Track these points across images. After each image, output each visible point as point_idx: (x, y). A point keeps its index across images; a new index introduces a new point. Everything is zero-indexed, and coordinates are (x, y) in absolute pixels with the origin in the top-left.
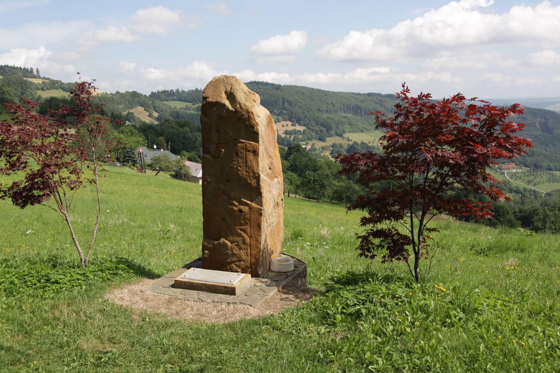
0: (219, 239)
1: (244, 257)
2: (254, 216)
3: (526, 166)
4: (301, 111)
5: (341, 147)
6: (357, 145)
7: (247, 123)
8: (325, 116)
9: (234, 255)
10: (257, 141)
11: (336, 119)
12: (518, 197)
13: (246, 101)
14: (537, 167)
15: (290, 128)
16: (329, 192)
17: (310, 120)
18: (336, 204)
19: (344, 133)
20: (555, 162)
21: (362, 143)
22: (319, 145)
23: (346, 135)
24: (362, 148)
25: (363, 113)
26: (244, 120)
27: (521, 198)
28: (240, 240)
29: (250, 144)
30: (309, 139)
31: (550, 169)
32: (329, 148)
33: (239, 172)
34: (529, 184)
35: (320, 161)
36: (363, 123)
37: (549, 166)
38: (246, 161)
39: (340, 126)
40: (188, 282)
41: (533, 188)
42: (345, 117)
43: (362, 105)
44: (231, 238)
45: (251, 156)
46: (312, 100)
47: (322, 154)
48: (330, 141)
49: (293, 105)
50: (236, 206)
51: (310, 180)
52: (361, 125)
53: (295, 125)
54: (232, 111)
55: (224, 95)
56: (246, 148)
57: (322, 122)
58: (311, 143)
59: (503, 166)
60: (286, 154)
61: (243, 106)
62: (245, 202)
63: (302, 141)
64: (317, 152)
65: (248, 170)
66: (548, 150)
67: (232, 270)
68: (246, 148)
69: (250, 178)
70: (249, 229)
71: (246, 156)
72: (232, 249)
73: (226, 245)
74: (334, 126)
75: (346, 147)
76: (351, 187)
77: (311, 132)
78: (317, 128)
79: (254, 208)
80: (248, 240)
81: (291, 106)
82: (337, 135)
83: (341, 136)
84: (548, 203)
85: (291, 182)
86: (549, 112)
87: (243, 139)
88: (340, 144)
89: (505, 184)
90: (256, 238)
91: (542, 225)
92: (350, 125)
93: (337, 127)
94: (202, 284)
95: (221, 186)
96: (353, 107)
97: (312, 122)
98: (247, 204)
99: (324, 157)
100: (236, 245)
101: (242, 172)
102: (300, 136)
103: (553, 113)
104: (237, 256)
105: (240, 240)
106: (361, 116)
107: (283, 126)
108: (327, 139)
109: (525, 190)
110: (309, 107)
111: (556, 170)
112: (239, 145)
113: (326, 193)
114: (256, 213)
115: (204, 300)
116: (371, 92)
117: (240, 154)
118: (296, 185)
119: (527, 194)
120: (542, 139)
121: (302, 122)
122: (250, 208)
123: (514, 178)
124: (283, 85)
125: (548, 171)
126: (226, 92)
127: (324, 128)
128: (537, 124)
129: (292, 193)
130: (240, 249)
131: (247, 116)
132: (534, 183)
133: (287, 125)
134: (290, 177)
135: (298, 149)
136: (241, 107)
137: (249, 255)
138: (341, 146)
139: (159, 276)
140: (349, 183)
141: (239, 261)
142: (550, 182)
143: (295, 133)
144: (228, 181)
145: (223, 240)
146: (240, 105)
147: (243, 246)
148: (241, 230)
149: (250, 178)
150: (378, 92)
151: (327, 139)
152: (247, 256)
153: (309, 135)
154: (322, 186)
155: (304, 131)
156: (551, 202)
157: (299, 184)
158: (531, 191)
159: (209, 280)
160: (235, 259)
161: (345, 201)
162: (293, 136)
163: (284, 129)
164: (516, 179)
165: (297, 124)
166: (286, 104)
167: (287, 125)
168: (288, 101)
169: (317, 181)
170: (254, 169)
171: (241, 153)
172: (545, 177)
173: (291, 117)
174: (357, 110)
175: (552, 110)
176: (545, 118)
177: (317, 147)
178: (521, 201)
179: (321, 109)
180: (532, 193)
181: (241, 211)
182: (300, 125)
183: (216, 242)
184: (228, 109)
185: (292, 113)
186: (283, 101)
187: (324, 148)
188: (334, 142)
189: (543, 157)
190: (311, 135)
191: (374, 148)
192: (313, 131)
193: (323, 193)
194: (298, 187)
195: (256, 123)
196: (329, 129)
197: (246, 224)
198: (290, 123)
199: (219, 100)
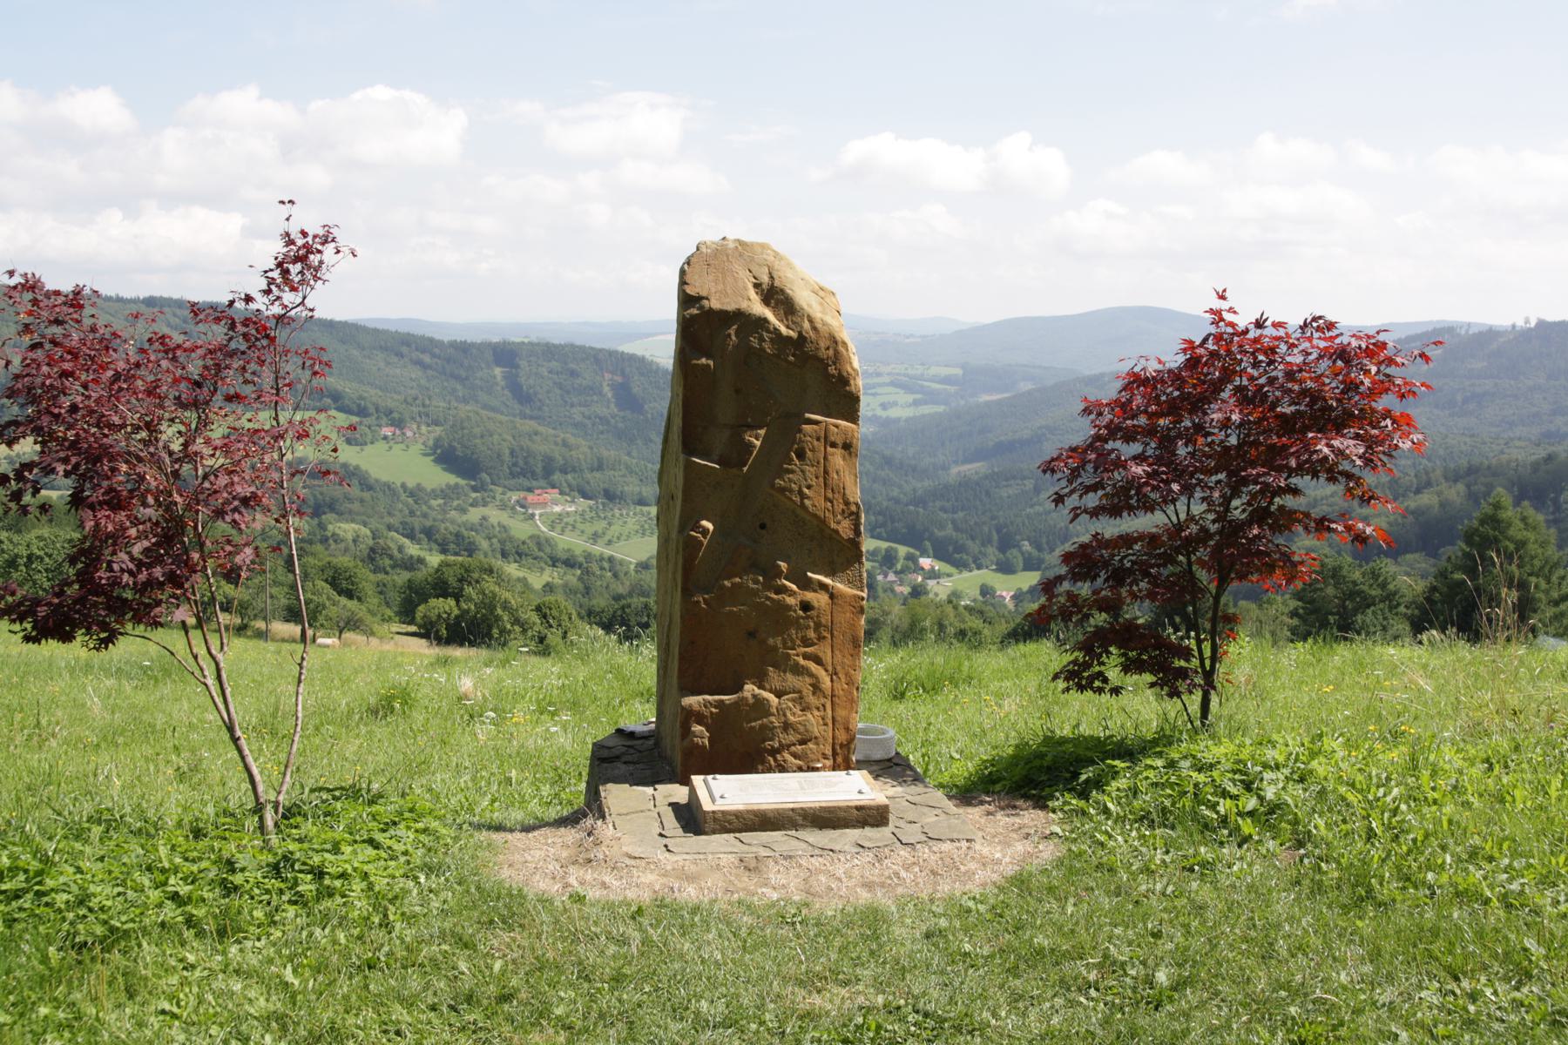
0: (741, 688)
1: (816, 730)
3: (585, 496)
7: (832, 370)
9: (787, 726)
10: (852, 416)
12: (573, 577)
13: (824, 312)
14: (611, 496)
26: (822, 364)
27: (580, 579)
28: (803, 683)
38: (826, 472)
41: (608, 552)
45: (837, 458)
50: (792, 594)
51: (17, 556)
54: (789, 338)
55: (752, 293)
59: (531, 497)
61: (819, 326)
65: (830, 495)
66: (634, 453)
67: (782, 769)
71: (825, 458)
72: (781, 712)
73: (760, 703)
79: (842, 595)
86: (632, 358)
89: (539, 545)
98: (824, 587)
100: (793, 700)
101: (816, 501)
103: (642, 360)
109: (588, 556)
112: (807, 427)
114: (848, 608)
116: (157, 294)
117: (809, 454)
119: (595, 567)
120: (621, 425)
122: (832, 596)
123: (558, 528)
126: (756, 286)
132: (607, 538)
136: (815, 329)
139: (918, 779)
141: (803, 742)
144: (763, 526)
146: (811, 321)
147: (812, 700)
148: (806, 656)
158: (602, 559)
164: (563, 532)
175: (639, 353)
176: (623, 373)
178: (581, 586)
180: (606, 565)
181: (806, 606)
197: (821, 638)
199: (744, 305)
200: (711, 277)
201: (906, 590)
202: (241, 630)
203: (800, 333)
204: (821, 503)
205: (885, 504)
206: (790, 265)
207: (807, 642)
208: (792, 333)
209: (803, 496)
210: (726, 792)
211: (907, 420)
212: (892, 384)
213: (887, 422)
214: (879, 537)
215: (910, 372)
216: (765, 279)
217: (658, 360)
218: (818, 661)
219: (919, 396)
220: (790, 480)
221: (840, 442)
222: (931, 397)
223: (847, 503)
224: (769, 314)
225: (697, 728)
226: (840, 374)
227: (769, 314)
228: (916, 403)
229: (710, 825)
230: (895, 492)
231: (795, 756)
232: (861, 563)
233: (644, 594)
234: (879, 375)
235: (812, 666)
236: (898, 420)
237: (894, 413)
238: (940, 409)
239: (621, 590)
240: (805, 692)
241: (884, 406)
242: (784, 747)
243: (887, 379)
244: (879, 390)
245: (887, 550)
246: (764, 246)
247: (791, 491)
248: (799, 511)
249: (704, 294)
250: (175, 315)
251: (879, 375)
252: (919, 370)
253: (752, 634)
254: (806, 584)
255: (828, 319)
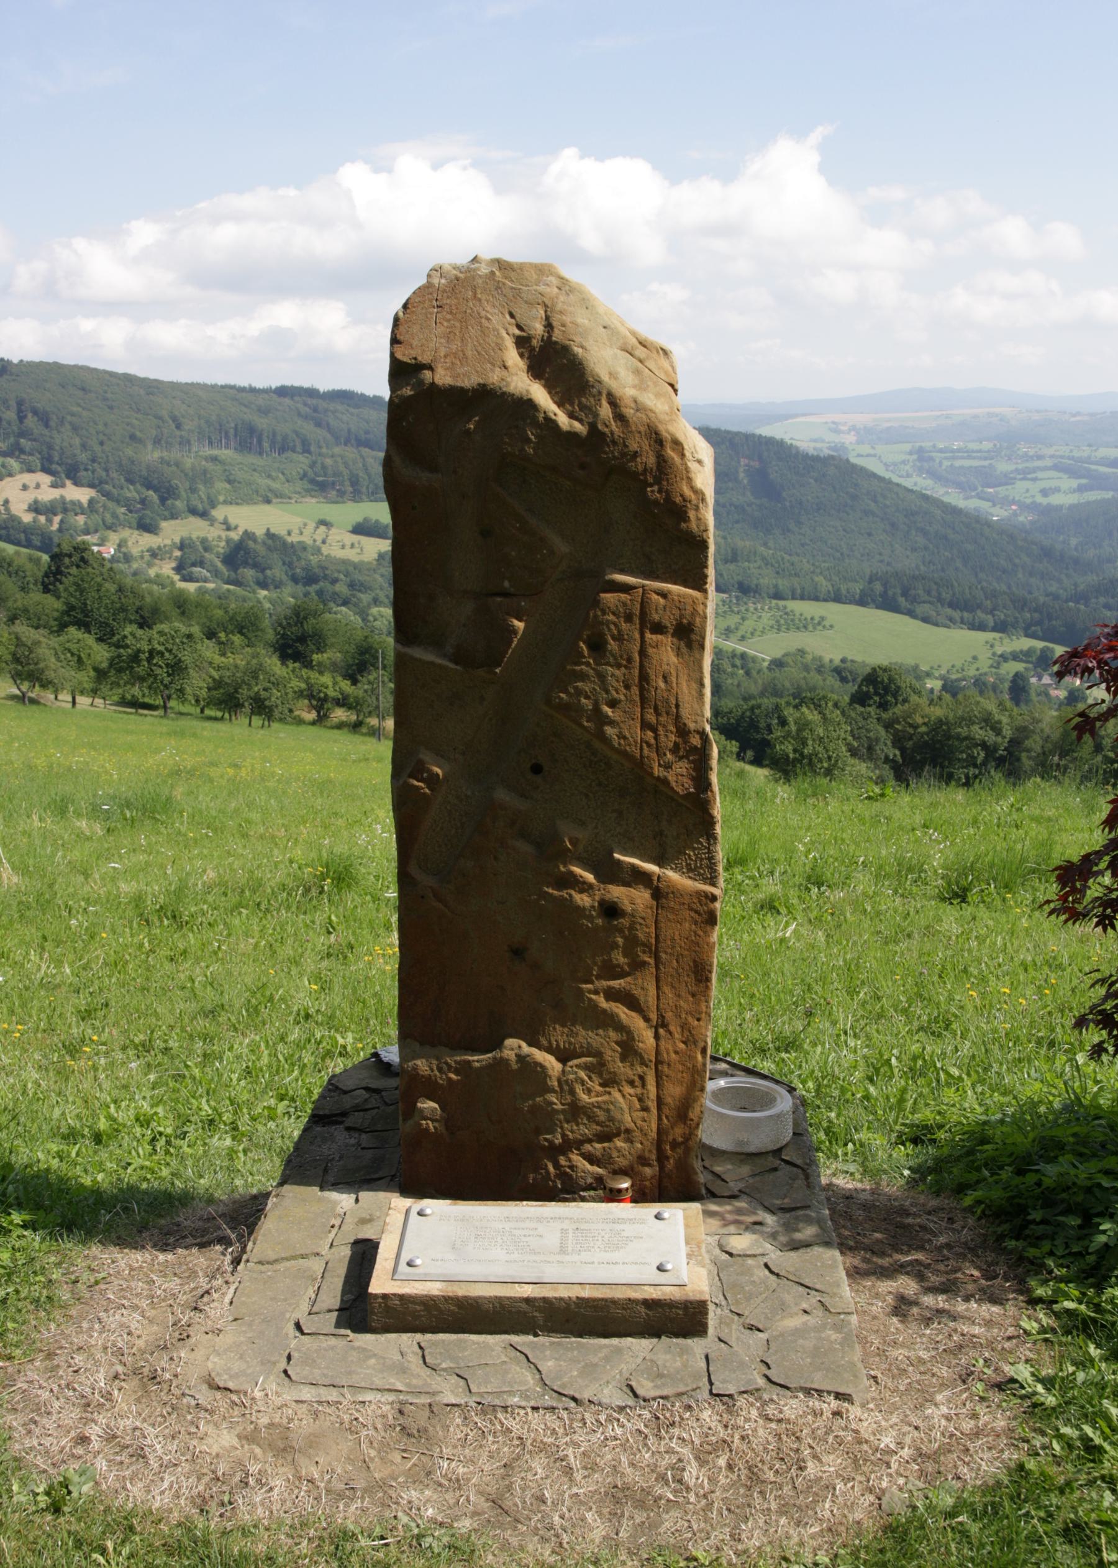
0: (498, 1045)
2: (677, 930)
4: (77, 441)
5: (206, 549)
6: (255, 541)
7: (653, 493)
8: (152, 455)
9: (576, 1111)
11: (188, 462)
13: (641, 386)
15: (48, 494)
16: (197, 683)
17: (107, 470)
18: (215, 719)
19: (213, 507)
20: (791, 575)
21: (269, 535)
22: (140, 542)
23: (219, 513)
24: (269, 549)
25: (266, 445)
26: (639, 481)
28: (606, 1042)
29: (664, 595)
30: (109, 528)
31: (778, 596)
32: (171, 552)
33: (609, 730)
34: (727, 638)
35: (151, 593)
36: (269, 476)
37: (776, 586)
38: (644, 677)
39: (201, 487)
40: (447, 1299)
41: (741, 648)
42: (214, 459)
43: (262, 423)
44: (559, 1035)
45: (666, 653)
46: (111, 408)
47: (152, 572)
48: (172, 531)
49: (52, 424)
50: (585, 887)
51: (139, 651)
52: (263, 482)
53: (63, 486)
54: (572, 435)
55: (512, 356)
56: (643, 613)
57: (144, 473)
58: (114, 538)
60: (46, 575)
61: (629, 412)
62: (634, 869)
63: (87, 532)
64: (135, 566)
65: (651, 718)
66: (771, 544)
68: (643, 613)
69: (660, 753)
70: (652, 991)
71: (643, 653)
72: (566, 1086)
73: (531, 1071)
74: (182, 486)
75: (221, 547)
76: (261, 667)
77: (111, 505)
78: (131, 493)
79: (676, 892)
80: (646, 1038)
81: (47, 426)
82: (193, 512)
83: (203, 515)
84: (779, 686)
85: (80, 660)
86: (770, 442)
87: (622, 571)
88: (204, 541)
90: (684, 1026)
91: (795, 751)
92: (229, 482)
93: (193, 490)
94: (527, 1300)
95: (502, 795)
96: (236, 429)
97: (115, 475)
98: (640, 878)
99: (159, 581)
100: (586, 1068)
101: (625, 728)
102: (81, 520)
103: (781, 444)
104: (592, 1118)
105: (606, 1042)
106: (261, 454)
107: (25, 488)
108: (164, 524)
110: (101, 427)
111: (793, 598)
112: (609, 598)
113: (188, 690)
114: (687, 914)
115: (585, 1395)
116: (288, 383)
117: (613, 645)
118: (95, 669)
121: (83, 473)
124: (15, 361)
125: (774, 602)
126: (522, 343)
127: (151, 492)
128: (742, 475)
129: (82, 693)
130: (610, 1082)
131: (651, 461)
132: (740, 633)
133: (38, 486)
134: (73, 647)
135: (82, 559)
136: (620, 417)
137: (652, 1105)
138: (206, 545)
140: (256, 656)
141: (605, 1137)
142: (779, 630)
143: (65, 510)
144: (537, 769)
145: (514, 1047)
146: (613, 402)
147: (622, 1069)
148: (612, 995)
149: (660, 753)
150: (306, 384)
151: (164, 524)
152: (645, 1109)
153: (108, 516)
154: (177, 668)
155: (91, 501)
156: (787, 684)
157: (105, 665)
158: (734, 655)
159: (552, 1272)
160: (585, 1130)
161: (247, 709)
162: (57, 519)
163: (30, 496)
165: (68, 483)
166: (31, 421)
167: (38, 486)
168: (35, 412)
169: (162, 654)
170: (685, 712)
171: (619, 638)
172: (767, 618)
173: (49, 459)
174: (248, 438)
177: (135, 551)
179: (138, 434)
180: (738, 662)
181: (611, 910)
182: (76, 484)
183: (478, 1060)
184: (550, 423)
185: (50, 447)
186: (20, 411)
187: (154, 554)
188: (185, 534)
189: (759, 563)
190: (115, 516)
191: (305, 549)
192: (118, 502)
193: (181, 691)
194: (101, 674)
195: (696, 491)
196: (167, 493)
197: (637, 966)
198: (46, 479)
199: (494, 378)
200: (440, 330)
201: (1062, 694)
202: (356, 727)
203: (593, 427)
204: (636, 732)
205: (1042, 599)
206: (586, 302)
207: (612, 971)
208: (578, 426)
209: (602, 720)
210: (440, 1243)
211: (1072, 507)
212: (1056, 468)
213: (1049, 510)
214: (1034, 636)
215: (1076, 454)
216: (538, 328)
217: (798, 444)
218: (633, 1003)
219: (1084, 481)
220: (579, 692)
221: (669, 621)
222: (1098, 482)
223: (683, 732)
224: (540, 395)
225: (428, 1105)
226: (668, 499)
227: (540, 395)
228: (1081, 489)
229: (375, 1320)
230: (1054, 587)
231: (591, 1159)
232: (711, 837)
233: (777, 693)
234: (1040, 457)
235: (622, 1012)
236: (1060, 508)
237: (1056, 500)
238: (1109, 495)
239: (754, 689)
240: (608, 1055)
241: (1045, 493)
242: (567, 1146)
243: (1048, 463)
244: (1040, 475)
245: (1043, 650)
246: (543, 270)
247: (580, 709)
248: (597, 744)
249: (424, 359)
250: (305, 405)
251: (1040, 457)
252: (1086, 452)
253: (518, 952)
254: (610, 873)
255: (649, 400)
